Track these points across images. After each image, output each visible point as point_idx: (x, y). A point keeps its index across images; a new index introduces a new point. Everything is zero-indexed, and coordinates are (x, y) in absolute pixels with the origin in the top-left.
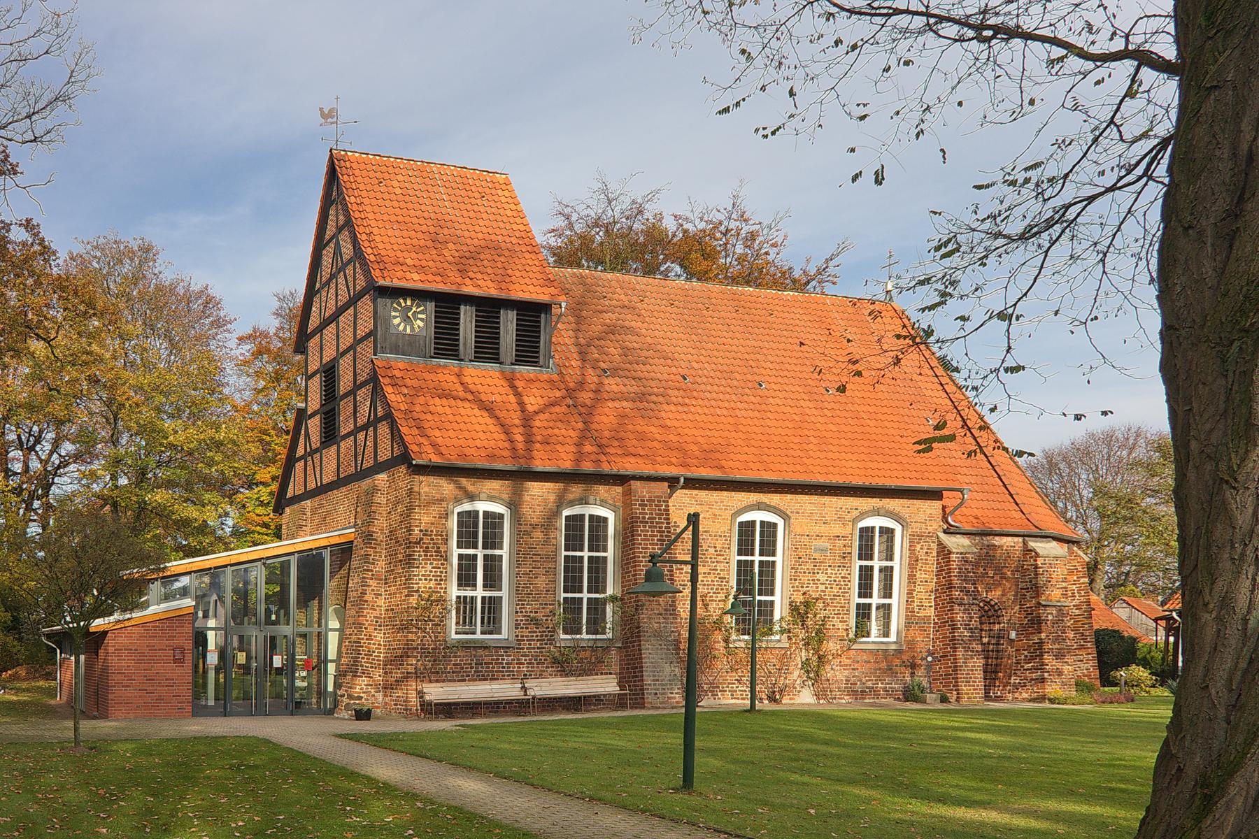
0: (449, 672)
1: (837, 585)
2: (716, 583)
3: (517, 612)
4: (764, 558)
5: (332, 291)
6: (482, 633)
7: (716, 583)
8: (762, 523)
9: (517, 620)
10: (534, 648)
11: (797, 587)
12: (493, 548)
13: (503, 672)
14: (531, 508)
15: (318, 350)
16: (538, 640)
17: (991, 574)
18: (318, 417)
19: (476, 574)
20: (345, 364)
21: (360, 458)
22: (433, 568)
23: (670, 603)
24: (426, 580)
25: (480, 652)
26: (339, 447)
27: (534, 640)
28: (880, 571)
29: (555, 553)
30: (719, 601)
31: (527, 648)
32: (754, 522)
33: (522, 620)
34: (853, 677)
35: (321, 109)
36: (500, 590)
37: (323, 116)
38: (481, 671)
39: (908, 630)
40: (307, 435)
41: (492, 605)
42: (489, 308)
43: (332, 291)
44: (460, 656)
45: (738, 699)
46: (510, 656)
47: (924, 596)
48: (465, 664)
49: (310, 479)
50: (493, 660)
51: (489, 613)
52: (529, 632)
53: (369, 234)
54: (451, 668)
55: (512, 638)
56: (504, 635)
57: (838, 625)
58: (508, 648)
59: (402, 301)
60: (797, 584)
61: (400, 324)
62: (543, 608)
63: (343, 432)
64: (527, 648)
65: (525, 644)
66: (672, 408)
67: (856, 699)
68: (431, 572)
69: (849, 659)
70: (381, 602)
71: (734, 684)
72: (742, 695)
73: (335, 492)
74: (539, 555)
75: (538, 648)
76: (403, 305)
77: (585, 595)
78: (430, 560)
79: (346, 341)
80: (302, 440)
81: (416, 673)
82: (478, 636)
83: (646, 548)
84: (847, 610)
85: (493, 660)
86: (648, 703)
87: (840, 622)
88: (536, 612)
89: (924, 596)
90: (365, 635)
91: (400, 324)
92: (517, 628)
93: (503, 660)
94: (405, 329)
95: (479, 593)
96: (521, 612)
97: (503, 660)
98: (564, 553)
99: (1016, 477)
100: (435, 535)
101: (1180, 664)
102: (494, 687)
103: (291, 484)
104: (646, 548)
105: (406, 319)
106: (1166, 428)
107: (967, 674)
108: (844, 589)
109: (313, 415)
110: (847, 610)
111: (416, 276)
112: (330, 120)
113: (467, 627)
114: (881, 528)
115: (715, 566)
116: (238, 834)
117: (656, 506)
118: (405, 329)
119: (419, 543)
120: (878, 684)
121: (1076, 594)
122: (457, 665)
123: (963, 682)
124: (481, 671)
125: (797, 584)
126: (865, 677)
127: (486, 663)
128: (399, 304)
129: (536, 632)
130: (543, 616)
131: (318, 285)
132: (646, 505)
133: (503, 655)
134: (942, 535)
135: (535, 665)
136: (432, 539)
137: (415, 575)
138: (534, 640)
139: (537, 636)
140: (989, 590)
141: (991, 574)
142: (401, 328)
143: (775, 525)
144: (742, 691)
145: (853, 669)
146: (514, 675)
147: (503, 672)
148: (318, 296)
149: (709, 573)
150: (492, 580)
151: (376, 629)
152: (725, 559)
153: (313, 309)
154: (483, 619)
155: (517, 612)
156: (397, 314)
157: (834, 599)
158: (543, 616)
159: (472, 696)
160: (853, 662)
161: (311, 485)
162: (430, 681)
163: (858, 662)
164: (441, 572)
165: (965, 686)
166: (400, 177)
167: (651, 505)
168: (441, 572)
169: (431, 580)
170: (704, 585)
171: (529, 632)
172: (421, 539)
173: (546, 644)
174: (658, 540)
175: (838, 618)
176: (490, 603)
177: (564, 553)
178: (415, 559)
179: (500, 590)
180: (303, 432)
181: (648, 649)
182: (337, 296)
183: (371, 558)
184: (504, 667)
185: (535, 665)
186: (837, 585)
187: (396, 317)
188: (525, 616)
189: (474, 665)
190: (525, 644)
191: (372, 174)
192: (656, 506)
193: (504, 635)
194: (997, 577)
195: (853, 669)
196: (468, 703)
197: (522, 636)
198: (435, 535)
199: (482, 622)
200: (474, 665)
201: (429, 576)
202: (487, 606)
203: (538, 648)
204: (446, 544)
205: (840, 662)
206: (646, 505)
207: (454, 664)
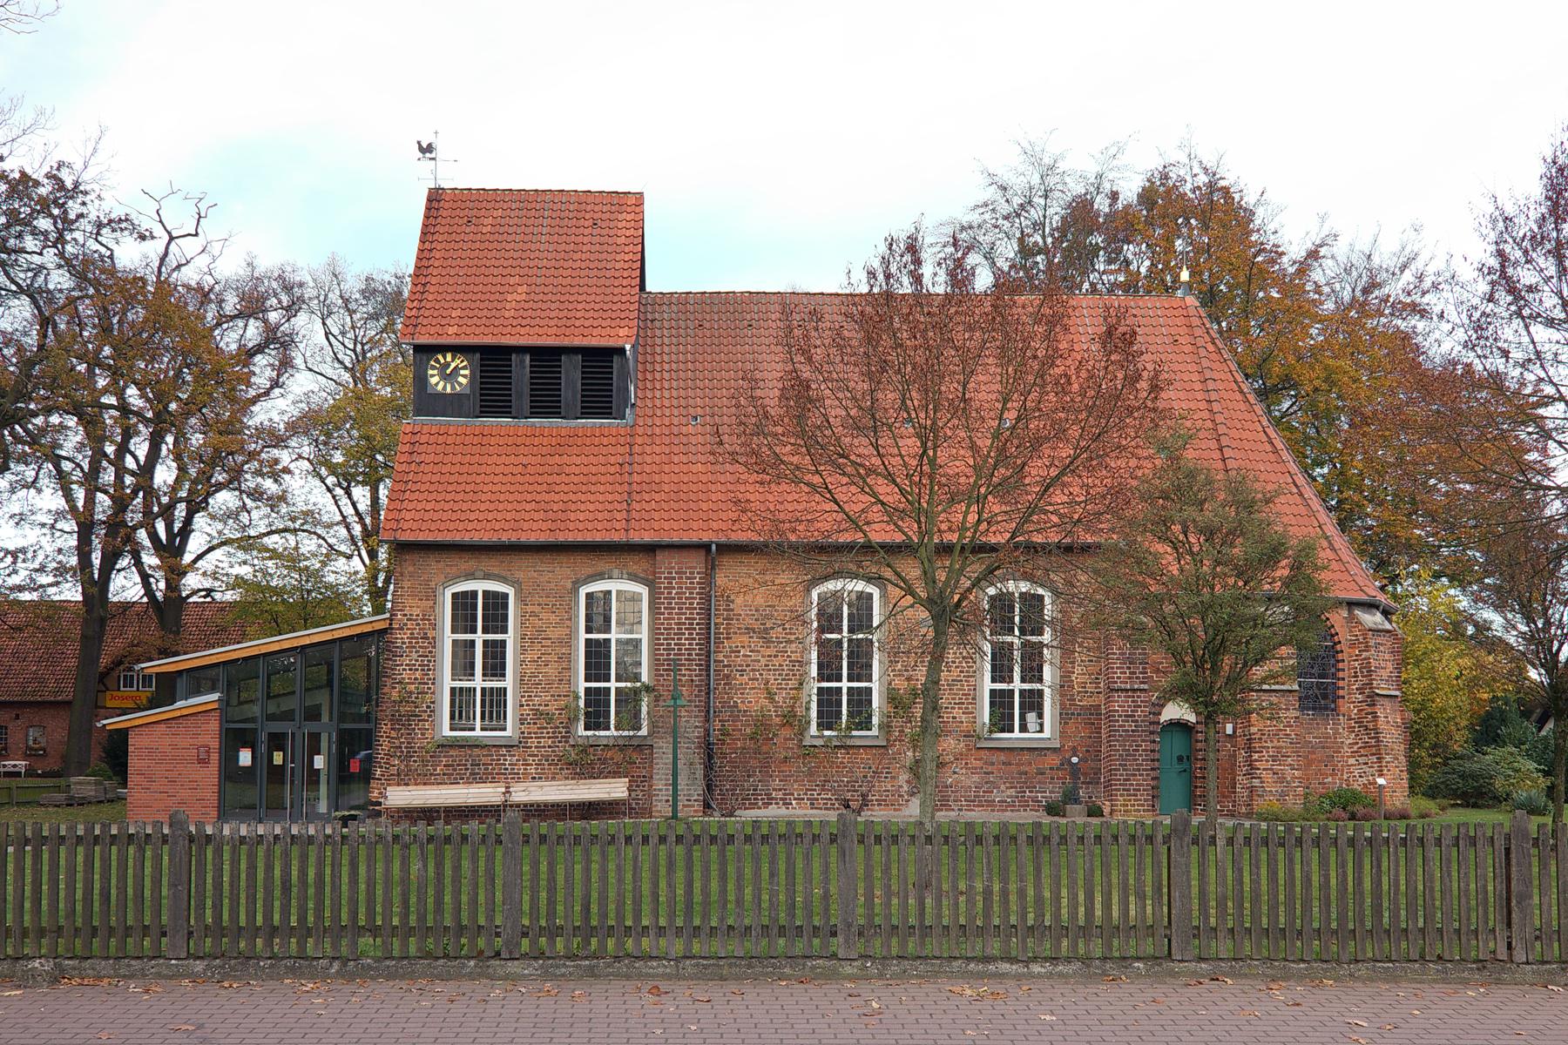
0: (439, 774)
1: (957, 667)
2: (785, 668)
3: (522, 706)
6: (482, 729)
7: (785, 668)
9: (522, 715)
10: (544, 747)
11: (899, 671)
13: (505, 774)
14: (538, 586)
16: (549, 738)
19: (505, 663)
22: (419, 656)
23: (696, 692)
24: (410, 670)
25: (476, 751)
27: (544, 738)
30: (791, 689)
31: (536, 747)
32: (474, 594)
33: (529, 715)
34: (986, 783)
35: (419, 143)
37: (422, 150)
38: (479, 774)
39: (1066, 723)
41: (495, 700)
42: (547, 357)
44: (452, 756)
45: (821, 809)
46: (514, 756)
48: (458, 765)
50: (494, 760)
51: (492, 706)
52: (538, 728)
54: (442, 770)
57: (960, 717)
58: (512, 746)
60: (899, 667)
61: (438, 383)
62: (556, 700)
64: (536, 747)
65: (533, 742)
67: (993, 811)
68: (417, 661)
69: (979, 760)
71: (815, 790)
72: (827, 804)
74: (550, 639)
75: (549, 747)
77: (845, 685)
78: (415, 647)
81: (399, 775)
82: (478, 733)
83: (670, 629)
84: (973, 699)
85: (494, 760)
86: (657, 811)
87: (963, 713)
88: (545, 705)
90: (385, 732)
91: (438, 383)
92: (522, 724)
93: (506, 760)
94: (445, 388)
95: (478, 682)
96: (528, 705)
97: (506, 760)
100: (422, 620)
102: (471, 791)
104: (670, 629)
105: (445, 377)
106: (158, 467)
107: (1125, 780)
108: (967, 672)
110: (973, 699)
112: (428, 155)
113: (494, 723)
114: (484, 592)
115: (785, 647)
117: (688, 578)
118: (445, 388)
119: (402, 629)
120: (1025, 792)
121: (1359, 674)
122: (449, 766)
123: (1119, 790)
124: (479, 774)
125: (899, 667)
126: (1005, 783)
127: (483, 765)
128: (437, 361)
129: (546, 728)
130: (556, 709)
132: (674, 578)
133: (505, 755)
135: (546, 767)
136: (419, 624)
137: (398, 665)
138: (544, 738)
139: (548, 733)
142: (440, 388)
144: (826, 799)
145: (985, 773)
146: (519, 778)
147: (505, 774)
149: (776, 656)
150: (495, 667)
152: (797, 638)
155: (522, 706)
156: (435, 372)
157: (954, 685)
158: (556, 709)
159: (441, 801)
160: (986, 763)
162: (416, 784)
163: (993, 764)
164: (429, 661)
165: (1121, 795)
168: (429, 661)
169: (417, 670)
170: (770, 670)
171: (538, 728)
173: (560, 742)
174: (686, 619)
175: (959, 708)
176: (492, 695)
178: (397, 647)
181: (662, 748)
184: (507, 769)
185: (546, 767)
186: (957, 667)
188: (532, 710)
189: (469, 766)
190: (533, 742)
192: (688, 578)
193: (508, 733)
195: (985, 773)
197: (530, 733)
198: (422, 620)
199: (483, 718)
200: (469, 766)
201: (415, 665)
202: (487, 699)
203: (549, 747)
205: (966, 764)
207: (445, 766)
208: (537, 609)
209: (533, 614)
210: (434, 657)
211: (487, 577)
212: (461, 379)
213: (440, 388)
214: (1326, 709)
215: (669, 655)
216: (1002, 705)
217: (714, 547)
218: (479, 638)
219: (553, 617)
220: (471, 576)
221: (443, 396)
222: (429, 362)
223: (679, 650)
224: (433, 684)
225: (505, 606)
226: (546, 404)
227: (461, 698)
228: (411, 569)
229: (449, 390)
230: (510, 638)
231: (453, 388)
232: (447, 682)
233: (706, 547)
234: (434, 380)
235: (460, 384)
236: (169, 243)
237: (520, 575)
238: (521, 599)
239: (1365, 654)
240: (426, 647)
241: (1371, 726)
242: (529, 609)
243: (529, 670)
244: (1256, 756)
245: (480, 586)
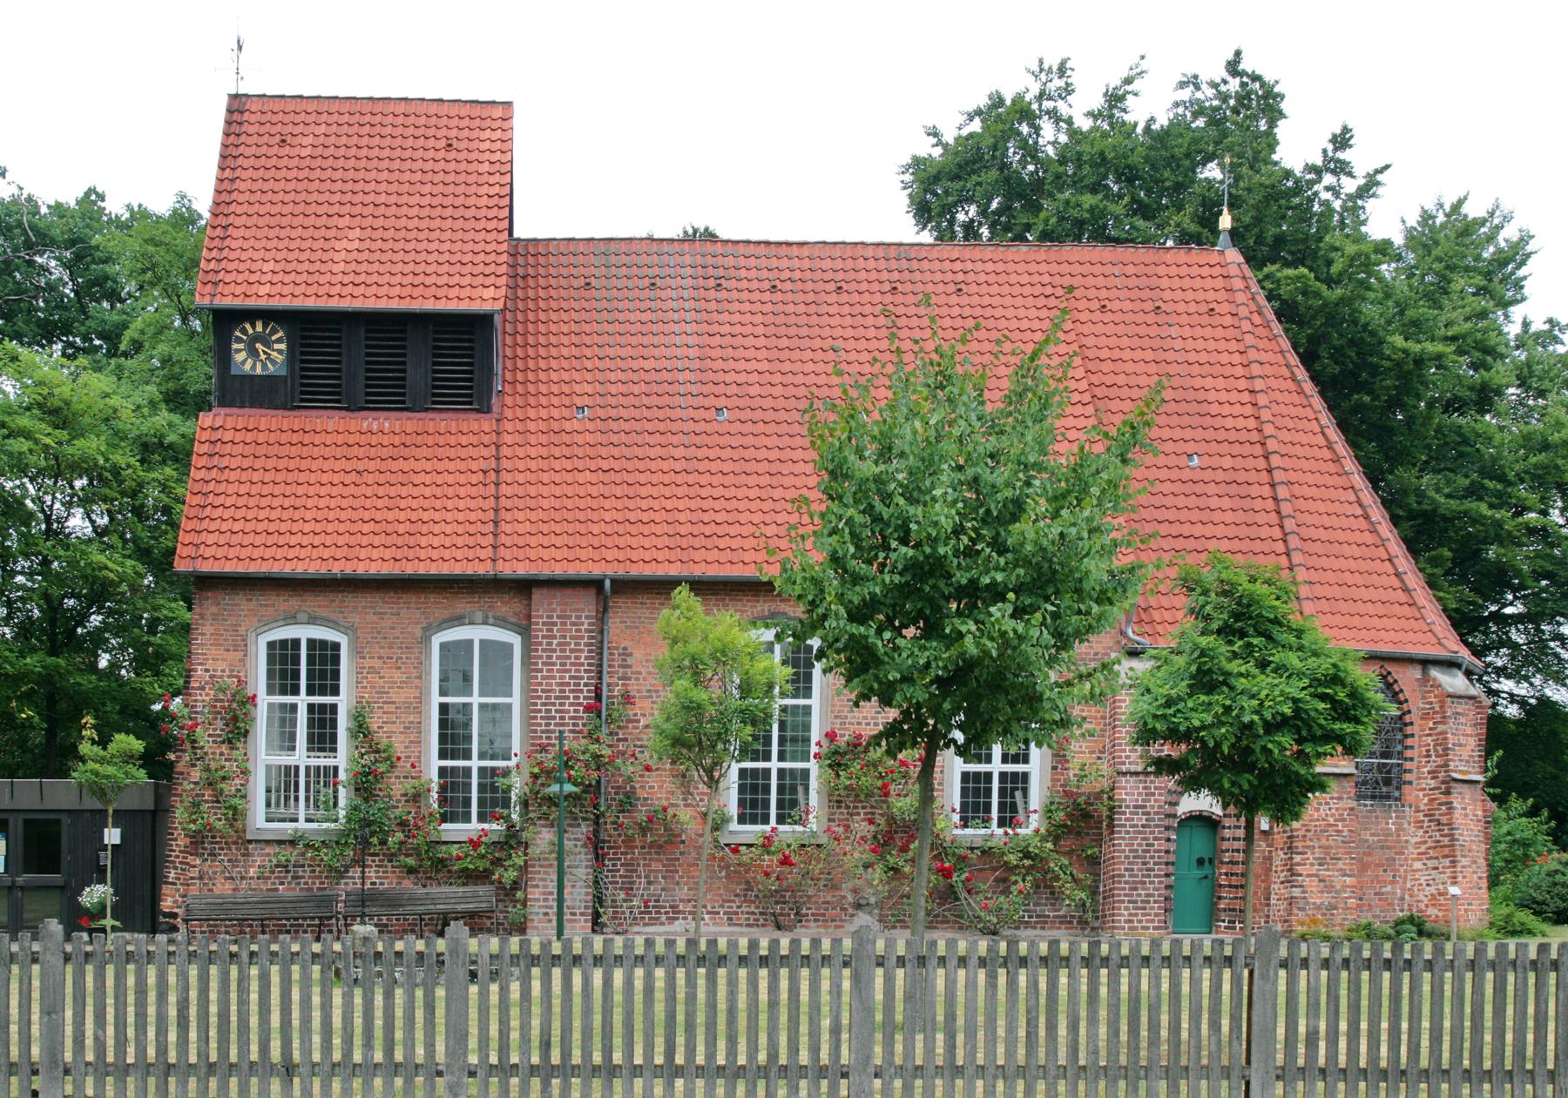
4: (317, 699)
8: (312, 643)
12: (283, 706)
28: (465, 705)
32: (296, 643)
59: (248, 326)
66: (475, 466)
70: (631, 768)
76: (251, 331)
105: (253, 353)
117: (573, 624)
128: (244, 331)
132: (555, 624)
143: (336, 646)
156: (241, 346)
165: (1127, 908)
167: (564, 624)
187: (239, 351)
192: (573, 624)
206: (555, 624)
208: (377, 663)
209: (372, 670)
211: (313, 620)
214: (1388, 797)
217: (608, 583)
220: (292, 619)
225: (336, 659)
228: (214, 609)
229: (259, 371)
233: (595, 584)
234: (240, 357)
237: (355, 619)
238: (357, 652)
239: (1441, 728)
241: (1444, 820)
244: (1297, 858)
245: (304, 633)
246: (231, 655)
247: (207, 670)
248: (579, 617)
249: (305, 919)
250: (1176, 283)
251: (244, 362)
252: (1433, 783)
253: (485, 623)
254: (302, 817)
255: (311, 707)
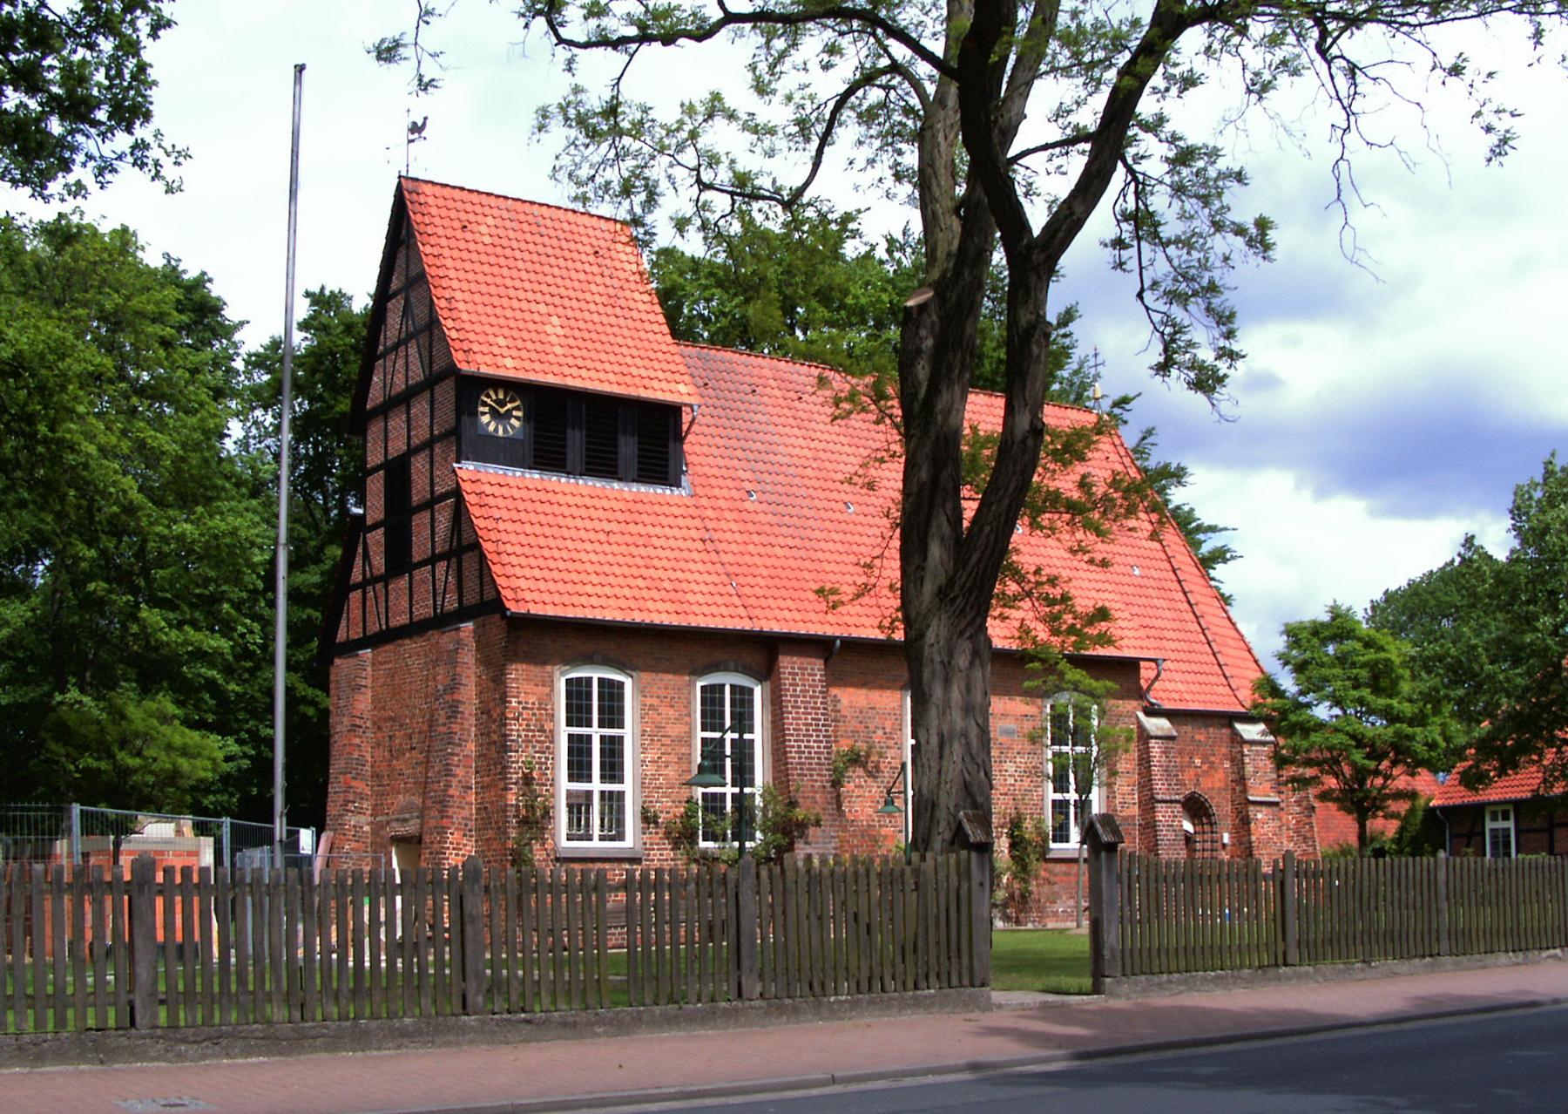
5: (401, 362)
15: (382, 437)
17: (1198, 762)
18: (381, 531)
20: (419, 464)
21: (439, 599)
26: (411, 578)
29: (690, 734)
36: (622, 781)
40: (366, 556)
43: (401, 362)
47: (1126, 789)
49: (371, 619)
53: (449, 300)
55: (639, 846)
56: (628, 842)
59: (492, 393)
63: (416, 558)
73: (407, 641)
79: (421, 434)
80: (359, 561)
82: (596, 844)
89: (1126, 789)
94: (496, 430)
95: (596, 786)
98: (700, 734)
99: (1230, 642)
101: (367, 964)
103: (343, 623)
109: (375, 527)
111: (509, 362)
116: (536, 972)
117: (810, 675)
118: (496, 430)
131: (381, 348)
134: (1141, 715)
136: (534, 714)
140: (1476, 705)
141: (1198, 762)
142: (501, 433)
148: (381, 361)
151: (465, 835)
153: (375, 379)
154: (602, 820)
156: (486, 409)
161: (373, 628)
164: (547, 758)
166: (490, 221)
167: (803, 674)
172: (520, 714)
177: (700, 734)
179: (622, 781)
180: (360, 550)
182: (407, 371)
183: (457, 737)
191: (453, 214)
194: (1205, 767)
196: (773, 722)
204: (552, 721)
208: (655, 702)
209: (652, 707)
210: (552, 753)
212: (513, 421)
213: (491, 428)
215: (800, 758)
216: (713, 810)
218: (596, 732)
219: (671, 712)
221: (493, 438)
222: (479, 397)
223: (810, 753)
224: (551, 785)
225: (621, 697)
226: (602, 465)
227: (579, 806)
228: (526, 649)
230: (628, 732)
231: (505, 430)
232: (564, 785)
234: (485, 419)
235: (513, 427)
236: (1330, 68)
240: (543, 742)
241: (1309, 835)
242: (649, 701)
243: (651, 770)
246: (540, 689)
247: (519, 703)
248: (813, 669)
249: (616, 927)
250: (465, 286)
251: (488, 423)
252: (1298, 809)
253: (736, 671)
254: (596, 837)
255: (602, 738)
